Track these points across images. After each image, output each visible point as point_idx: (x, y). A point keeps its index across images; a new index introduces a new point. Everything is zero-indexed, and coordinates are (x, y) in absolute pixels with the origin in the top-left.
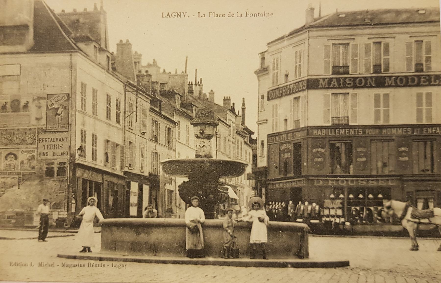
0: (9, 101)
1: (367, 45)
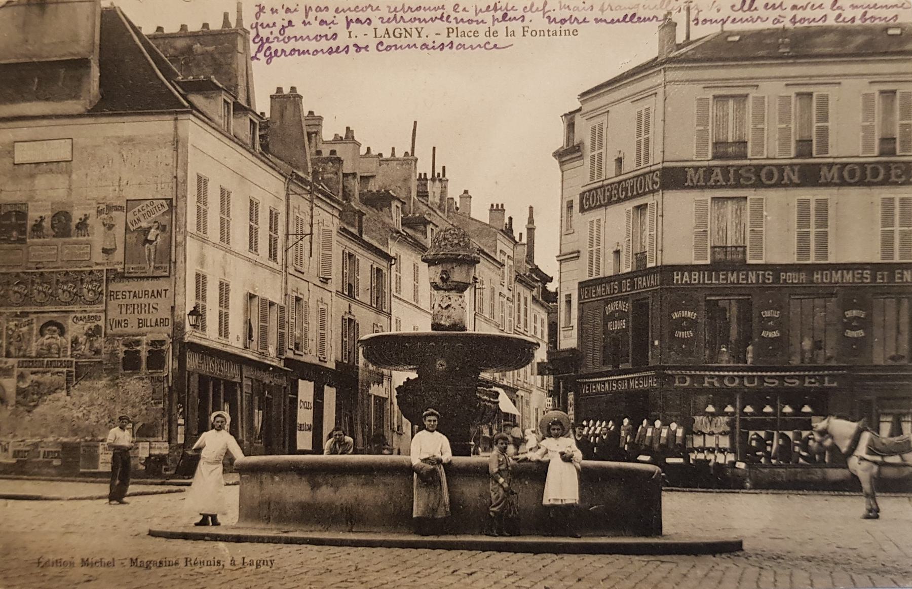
0: (48, 214)
1: (785, 99)
